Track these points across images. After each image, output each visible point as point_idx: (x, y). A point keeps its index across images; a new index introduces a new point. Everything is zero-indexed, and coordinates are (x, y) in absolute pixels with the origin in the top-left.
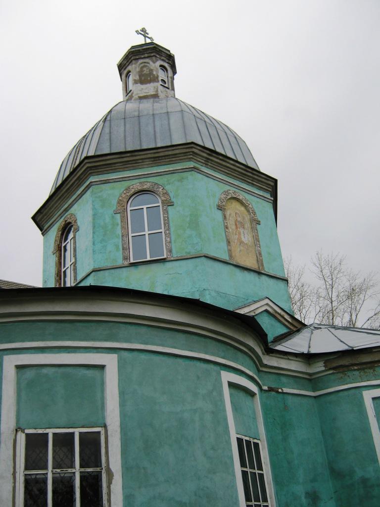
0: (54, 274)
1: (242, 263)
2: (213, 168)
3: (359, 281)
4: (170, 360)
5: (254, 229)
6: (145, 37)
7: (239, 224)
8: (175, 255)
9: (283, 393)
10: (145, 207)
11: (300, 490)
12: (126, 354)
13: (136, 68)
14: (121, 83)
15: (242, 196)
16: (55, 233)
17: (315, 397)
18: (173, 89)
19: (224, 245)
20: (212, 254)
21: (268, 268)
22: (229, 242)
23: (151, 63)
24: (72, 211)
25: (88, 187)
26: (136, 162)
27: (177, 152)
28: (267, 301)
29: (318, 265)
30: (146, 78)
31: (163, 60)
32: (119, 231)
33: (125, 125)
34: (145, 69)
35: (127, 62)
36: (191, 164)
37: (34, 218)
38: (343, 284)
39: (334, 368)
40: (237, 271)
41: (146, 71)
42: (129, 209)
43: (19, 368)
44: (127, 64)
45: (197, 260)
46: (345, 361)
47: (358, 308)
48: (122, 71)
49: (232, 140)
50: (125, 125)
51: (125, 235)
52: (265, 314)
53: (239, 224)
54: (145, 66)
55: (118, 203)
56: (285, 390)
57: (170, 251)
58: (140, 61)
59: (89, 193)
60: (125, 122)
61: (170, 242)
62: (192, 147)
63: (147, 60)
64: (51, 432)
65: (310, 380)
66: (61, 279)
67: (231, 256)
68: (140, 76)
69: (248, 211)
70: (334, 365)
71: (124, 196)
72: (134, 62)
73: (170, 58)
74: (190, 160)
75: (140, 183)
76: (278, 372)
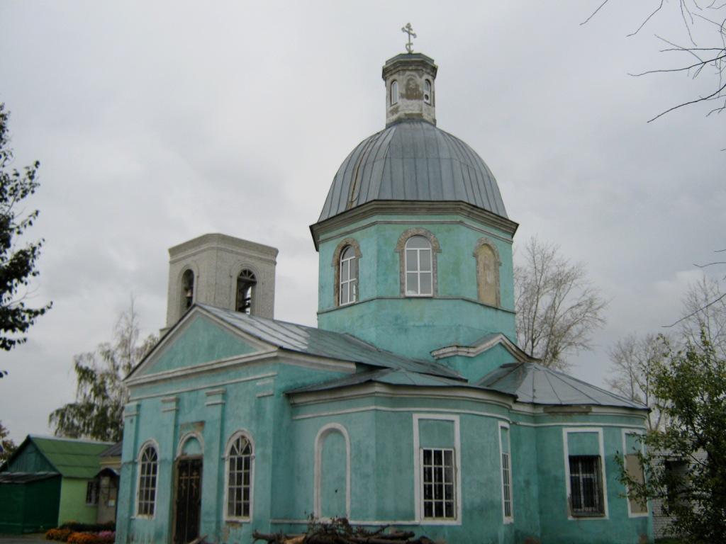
0: (333, 285)
1: (486, 302)
2: (473, 219)
3: (567, 270)
4: (479, 418)
5: (496, 270)
6: (409, 34)
7: (486, 267)
8: (440, 294)
9: (520, 425)
10: (418, 249)
11: (521, 478)
12: (463, 415)
13: (403, 80)
14: (385, 89)
15: (491, 241)
16: (334, 249)
17: (535, 427)
18: (434, 106)
19: (474, 287)
20: (467, 297)
21: (504, 305)
22: (478, 285)
23: (418, 77)
24: (357, 235)
25: (374, 224)
26: (414, 209)
27: (448, 206)
28: (502, 336)
29: (531, 250)
30: (412, 93)
31: (429, 74)
32: (397, 268)
33: (403, 166)
34: (411, 82)
35: (394, 69)
36: (459, 218)
37: (311, 227)
38: (552, 270)
39: (549, 413)
40: (482, 308)
41: (412, 85)
42: (406, 249)
43: (420, 420)
44: (394, 71)
45: (457, 301)
46: (556, 410)
47: (563, 295)
48: (388, 75)
49: (486, 179)
50: (403, 166)
51: (402, 272)
52: (500, 349)
53: (486, 267)
54: (411, 79)
55: (398, 243)
56: (521, 423)
57: (436, 291)
58: (408, 73)
59: (373, 229)
60: (403, 163)
61: (437, 284)
62: (459, 205)
63: (414, 73)
64: (443, 450)
65: (533, 416)
66: (339, 290)
67: (479, 297)
68: (407, 90)
69: (494, 254)
70: (550, 411)
71: (403, 238)
72: (401, 72)
73: (434, 69)
74: (457, 214)
75: (416, 228)
76: (518, 413)
